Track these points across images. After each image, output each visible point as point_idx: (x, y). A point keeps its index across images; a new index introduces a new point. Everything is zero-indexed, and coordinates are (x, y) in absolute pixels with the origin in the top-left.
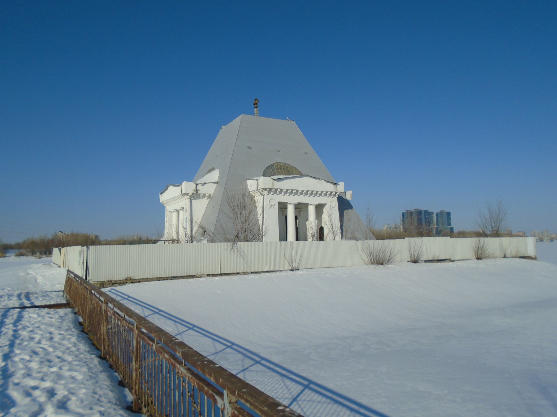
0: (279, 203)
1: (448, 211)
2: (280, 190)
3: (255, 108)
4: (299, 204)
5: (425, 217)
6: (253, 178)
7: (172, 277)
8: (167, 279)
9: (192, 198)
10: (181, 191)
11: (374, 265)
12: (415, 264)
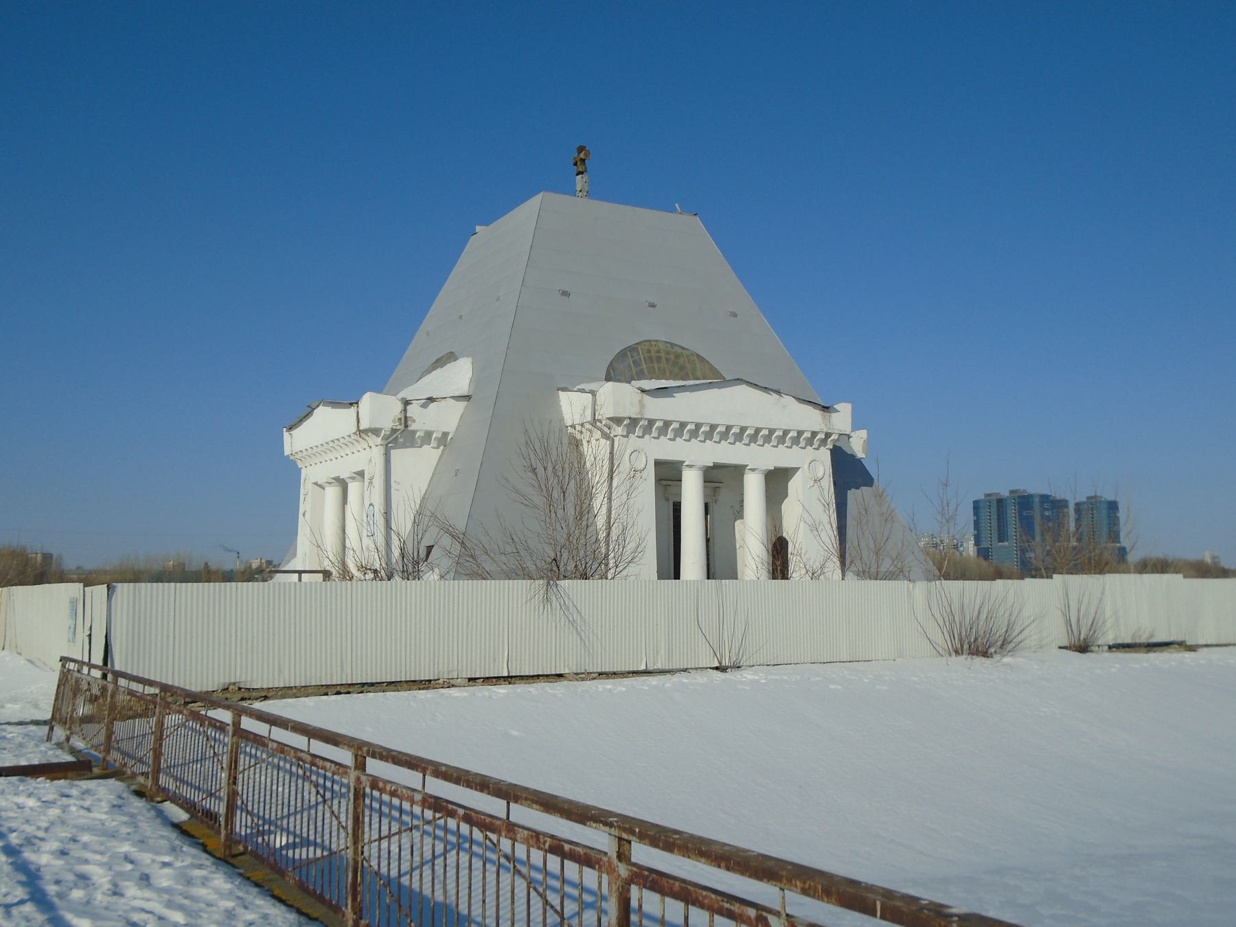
0: (658, 464)
1: (1111, 498)
2: (723, 429)
3: (577, 175)
4: (717, 467)
5: (1042, 516)
6: (578, 387)
7: (363, 685)
8: (351, 690)
9: (389, 443)
10: (358, 422)
11: (962, 658)
12: (1082, 655)
